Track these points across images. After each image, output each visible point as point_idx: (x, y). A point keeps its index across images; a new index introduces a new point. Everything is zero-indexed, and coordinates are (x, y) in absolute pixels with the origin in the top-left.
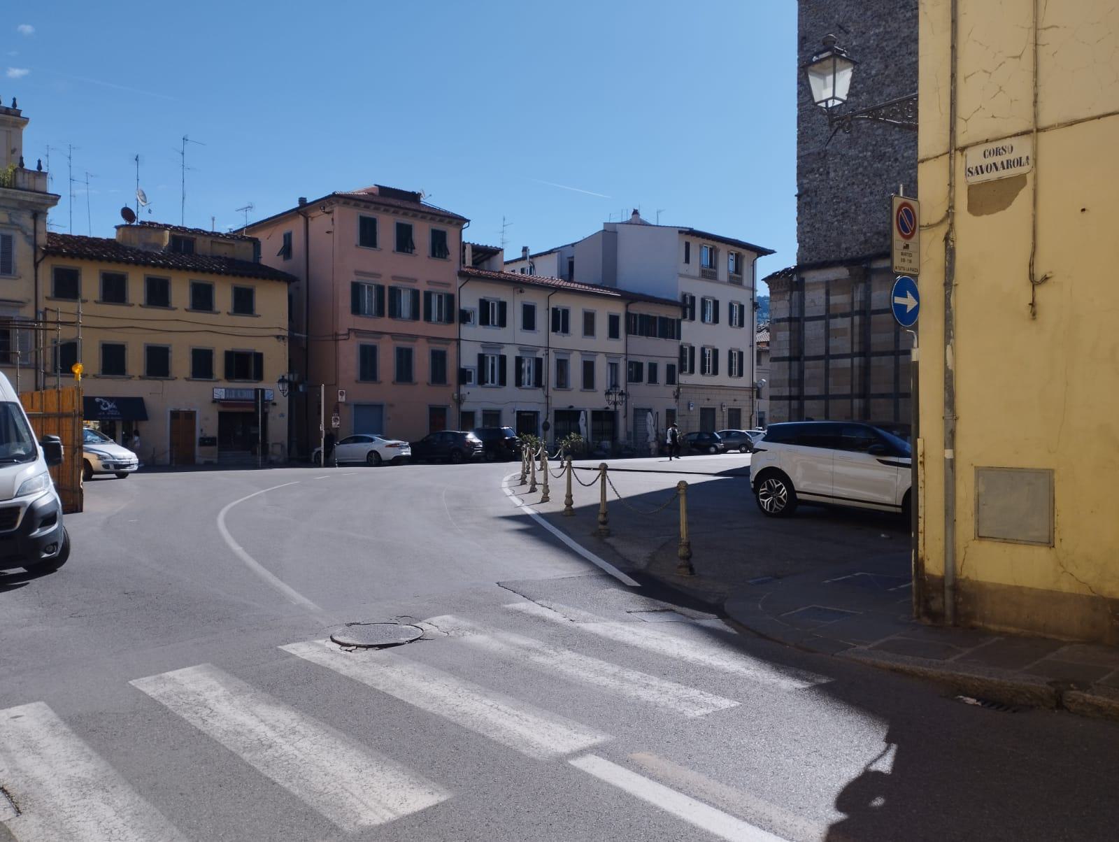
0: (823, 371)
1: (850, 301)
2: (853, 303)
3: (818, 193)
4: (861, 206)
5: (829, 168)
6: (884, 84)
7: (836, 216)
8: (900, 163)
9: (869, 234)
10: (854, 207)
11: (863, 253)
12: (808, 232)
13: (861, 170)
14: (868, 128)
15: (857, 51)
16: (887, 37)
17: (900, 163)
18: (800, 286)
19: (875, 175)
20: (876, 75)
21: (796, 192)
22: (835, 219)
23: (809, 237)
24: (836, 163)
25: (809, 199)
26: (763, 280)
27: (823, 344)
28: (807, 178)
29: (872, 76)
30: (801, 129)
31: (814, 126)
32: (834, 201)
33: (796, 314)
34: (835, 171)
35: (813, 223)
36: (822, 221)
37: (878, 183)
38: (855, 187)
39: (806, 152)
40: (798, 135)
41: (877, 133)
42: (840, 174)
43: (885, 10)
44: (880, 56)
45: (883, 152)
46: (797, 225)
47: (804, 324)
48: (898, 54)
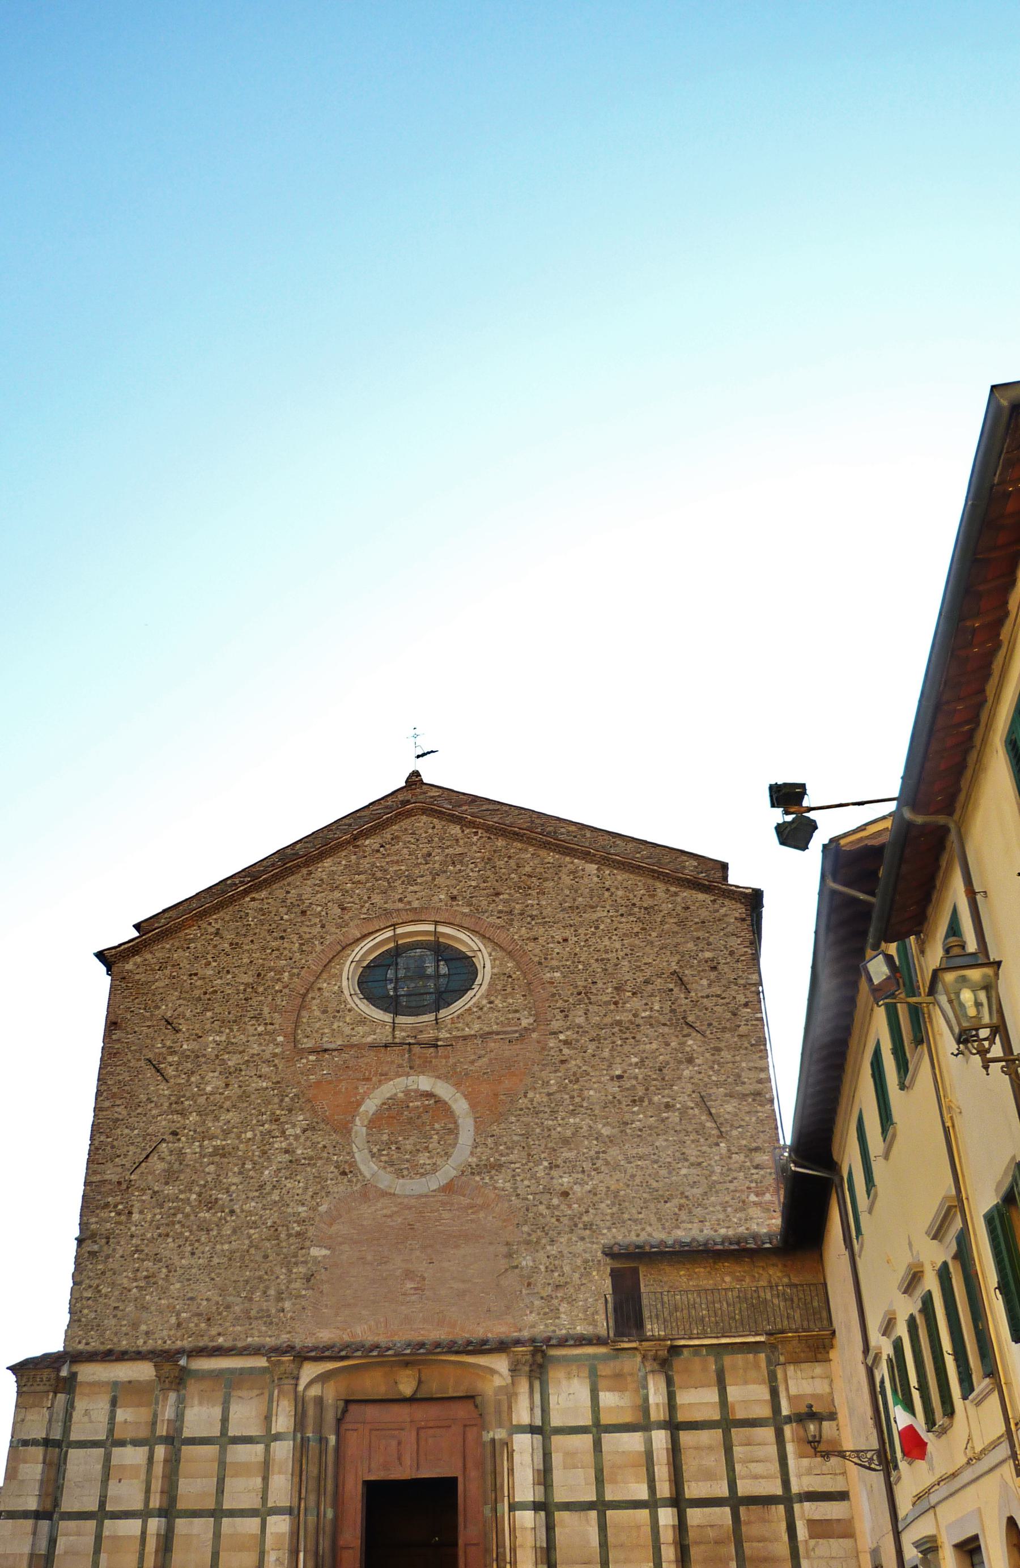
0: (91, 1540)
1: (150, 1419)
2: (154, 1423)
3: (111, 1240)
4: (175, 1271)
5: (132, 1206)
6: (221, 1107)
7: (136, 1280)
8: (238, 1216)
9: (184, 1315)
10: (164, 1270)
11: (173, 1342)
12: (89, 1299)
13: (180, 1216)
14: (196, 1161)
15: (188, 1057)
16: (231, 1048)
17: (238, 1216)
18: (69, 1386)
19: (200, 1229)
20: (212, 1094)
21: (77, 1234)
22: (135, 1284)
23: (88, 1307)
24: (144, 1201)
25: (96, 1248)
26: (8, 1368)
27: (96, 1491)
28: (97, 1216)
29: (206, 1094)
30: (96, 1143)
31: (115, 1143)
32: (136, 1256)
33: (57, 1435)
34: (141, 1212)
35: (98, 1286)
36: (113, 1284)
37: (203, 1239)
38: (170, 1240)
39: (98, 1178)
40: (90, 1150)
41: (207, 1170)
42: (149, 1216)
43: (231, 1016)
44: (219, 1069)
45: (214, 1197)
46: (72, 1285)
47: (67, 1452)
48: (243, 1073)
